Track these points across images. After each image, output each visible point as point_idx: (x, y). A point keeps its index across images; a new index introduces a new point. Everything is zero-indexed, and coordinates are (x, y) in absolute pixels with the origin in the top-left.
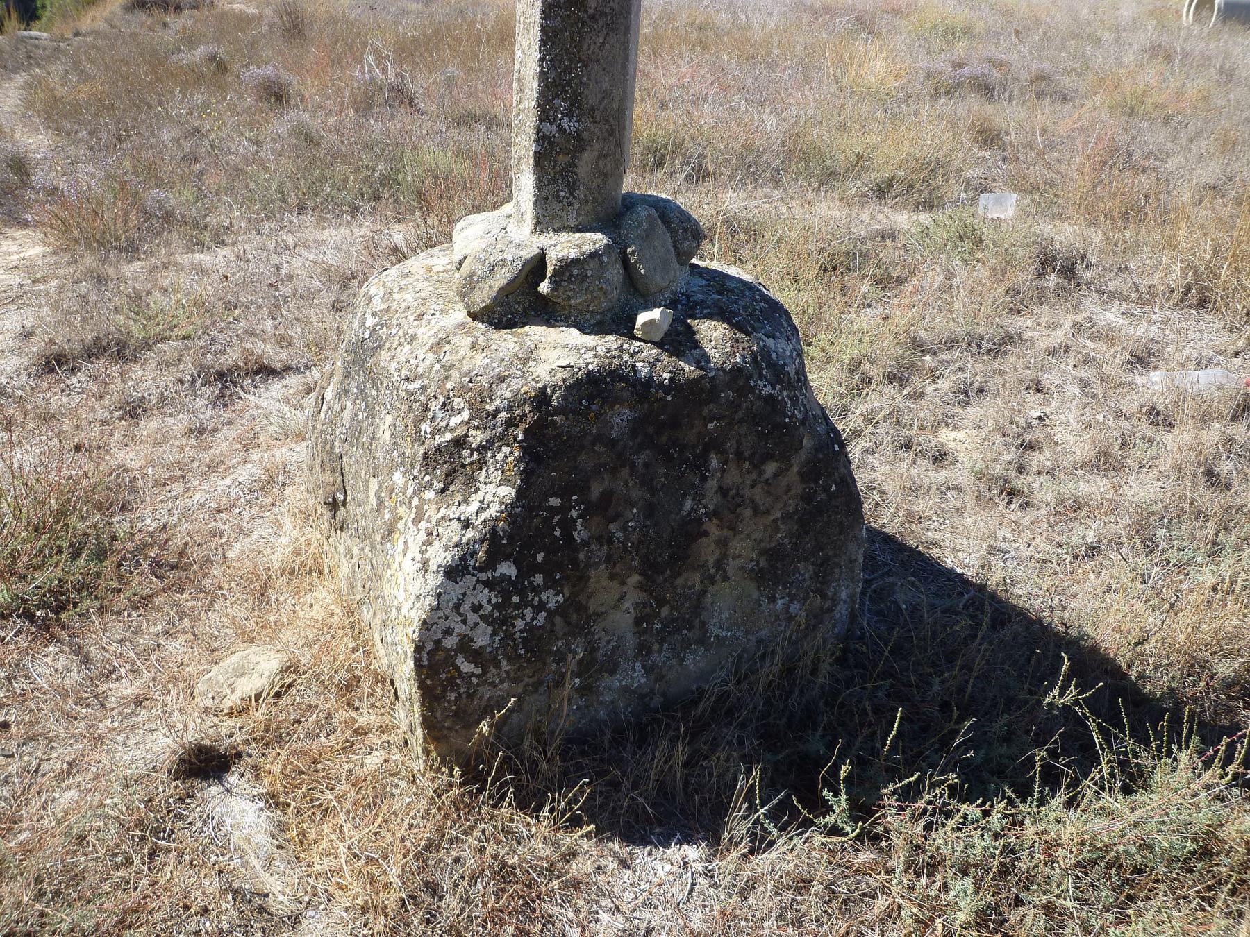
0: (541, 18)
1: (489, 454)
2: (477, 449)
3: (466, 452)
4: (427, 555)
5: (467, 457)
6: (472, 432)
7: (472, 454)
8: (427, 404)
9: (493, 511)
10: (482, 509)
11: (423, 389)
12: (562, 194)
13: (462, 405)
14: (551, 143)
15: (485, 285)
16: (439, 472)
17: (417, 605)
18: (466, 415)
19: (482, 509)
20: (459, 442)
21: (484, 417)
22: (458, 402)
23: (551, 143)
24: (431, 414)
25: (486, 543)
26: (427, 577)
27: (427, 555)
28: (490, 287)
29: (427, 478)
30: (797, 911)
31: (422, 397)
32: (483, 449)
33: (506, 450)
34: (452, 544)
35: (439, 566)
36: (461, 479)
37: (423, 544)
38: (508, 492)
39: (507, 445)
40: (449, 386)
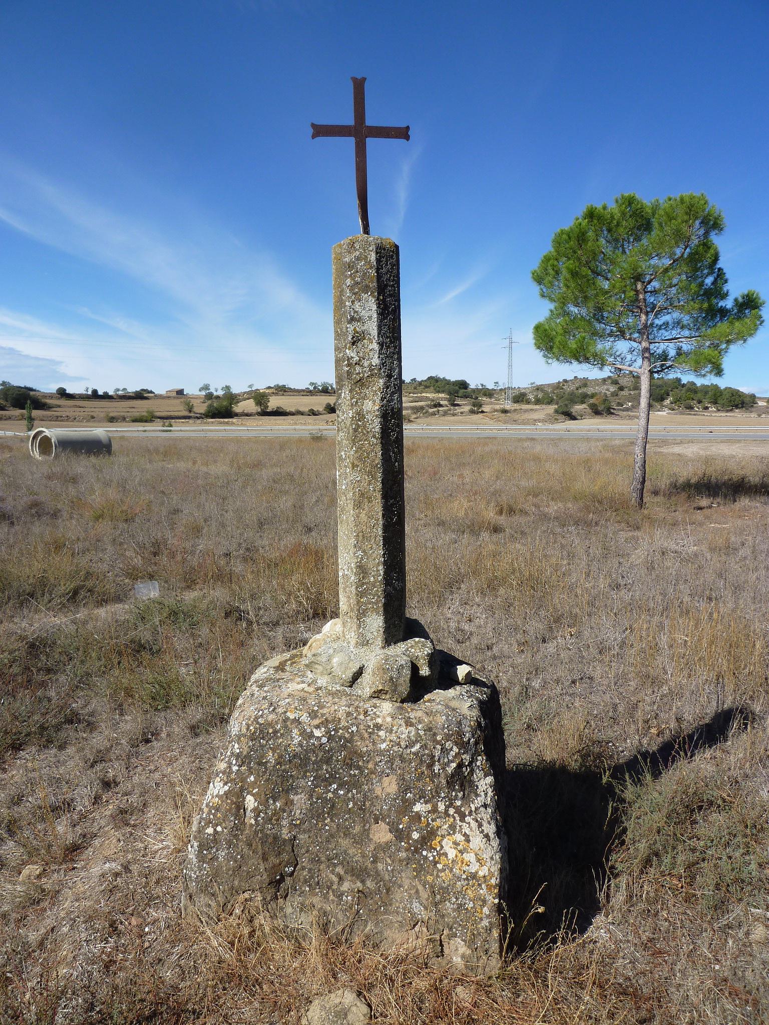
0: (383, 533)
1: (474, 765)
2: (468, 765)
3: (464, 769)
4: (486, 832)
5: (466, 771)
6: (463, 757)
7: (467, 769)
8: (432, 754)
9: (490, 794)
10: (486, 794)
11: (424, 747)
12: (397, 622)
13: (451, 745)
14: (390, 597)
15: (401, 680)
16: (457, 787)
17: (493, 862)
18: (456, 749)
19: (486, 794)
20: (460, 766)
21: (463, 746)
22: (448, 745)
23: (390, 597)
24: (437, 758)
25: (497, 810)
26: (492, 843)
27: (486, 832)
28: (404, 681)
29: (454, 794)
30: (694, 850)
31: (427, 752)
32: (471, 763)
33: (479, 758)
34: (490, 819)
35: (494, 833)
36: (467, 785)
37: (479, 828)
38: (490, 779)
39: (479, 755)
40: (439, 738)
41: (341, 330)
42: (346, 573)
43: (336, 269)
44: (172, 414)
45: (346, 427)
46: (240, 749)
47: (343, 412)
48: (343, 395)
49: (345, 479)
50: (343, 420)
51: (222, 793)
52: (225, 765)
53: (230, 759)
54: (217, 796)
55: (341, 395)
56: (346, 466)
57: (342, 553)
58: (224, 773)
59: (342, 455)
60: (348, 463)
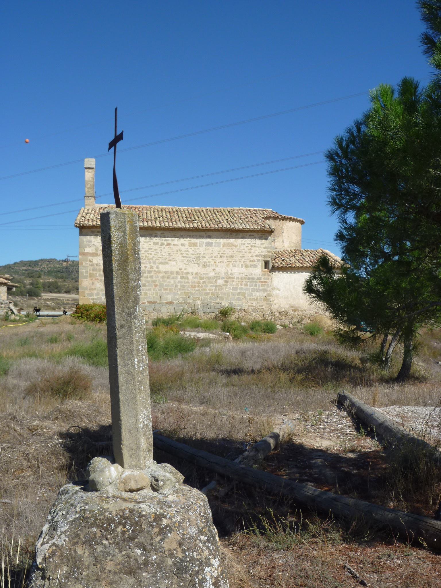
41: (135, 268)
42: (145, 423)
43: (130, 228)
44: (47, 318)
45: (141, 330)
46: (206, 536)
47: (139, 321)
48: (138, 309)
49: (142, 363)
50: (139, 326)
51: (219, 563)
52: (207, 551)
53: (206, 546)
54: (218, 567)
55: (136, 310)
56: (142, 355)
57: (141, 411)
58: (210, 555)
59: (139, 348)
60: (144, 353)
